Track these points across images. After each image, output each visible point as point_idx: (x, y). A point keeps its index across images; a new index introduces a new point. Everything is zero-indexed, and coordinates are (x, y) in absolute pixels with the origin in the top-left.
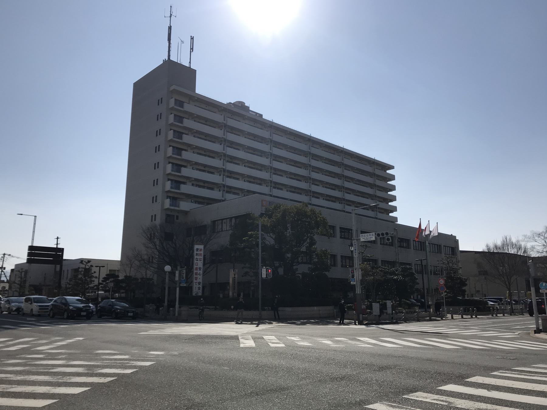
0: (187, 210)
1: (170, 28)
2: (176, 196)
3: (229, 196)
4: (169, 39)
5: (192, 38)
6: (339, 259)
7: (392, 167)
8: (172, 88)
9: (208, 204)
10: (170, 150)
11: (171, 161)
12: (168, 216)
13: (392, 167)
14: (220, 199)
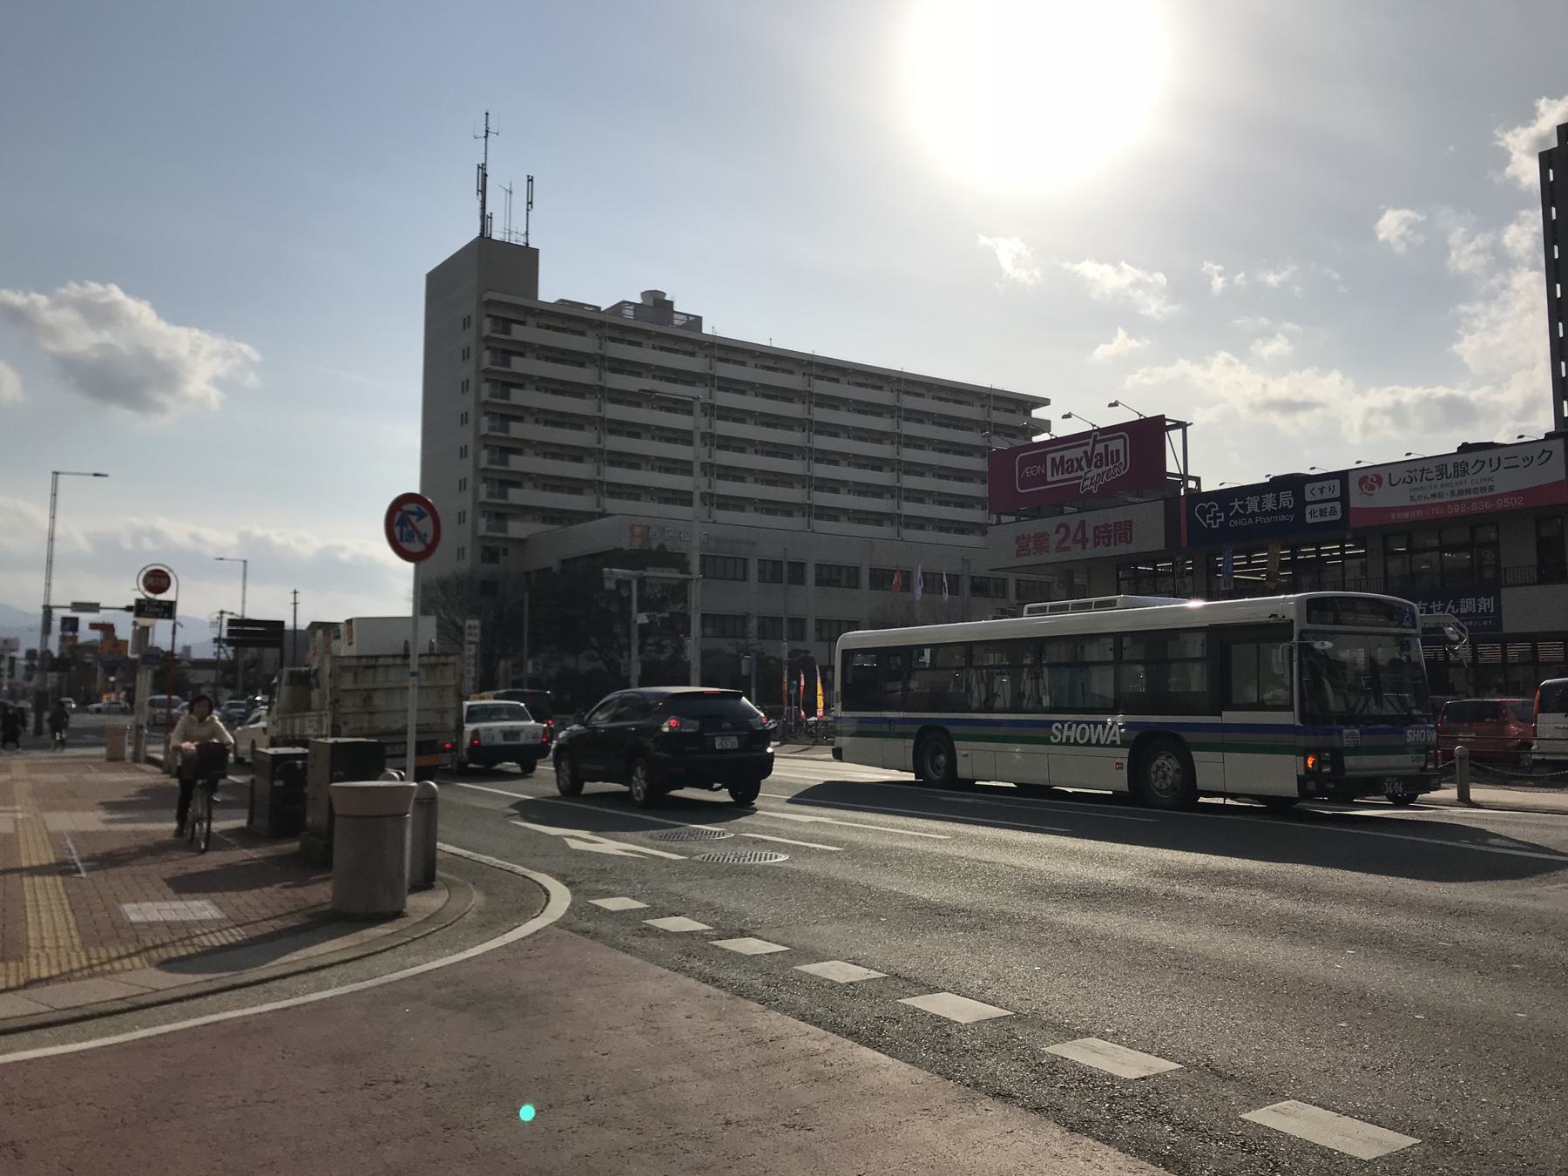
0: (523, 536)
1: (482, 168)
2: (501, 510)
3: (611, 504)
4: (483, 191)
5: (530, 180)
6: (811, 627)
7: (1045, 402)
8: (488, 296)
9: (571, 523)
10: (487, 323)
11: (490, 442)
12: (486, 549)
13: (1045, 402)
14: (589, 509)
